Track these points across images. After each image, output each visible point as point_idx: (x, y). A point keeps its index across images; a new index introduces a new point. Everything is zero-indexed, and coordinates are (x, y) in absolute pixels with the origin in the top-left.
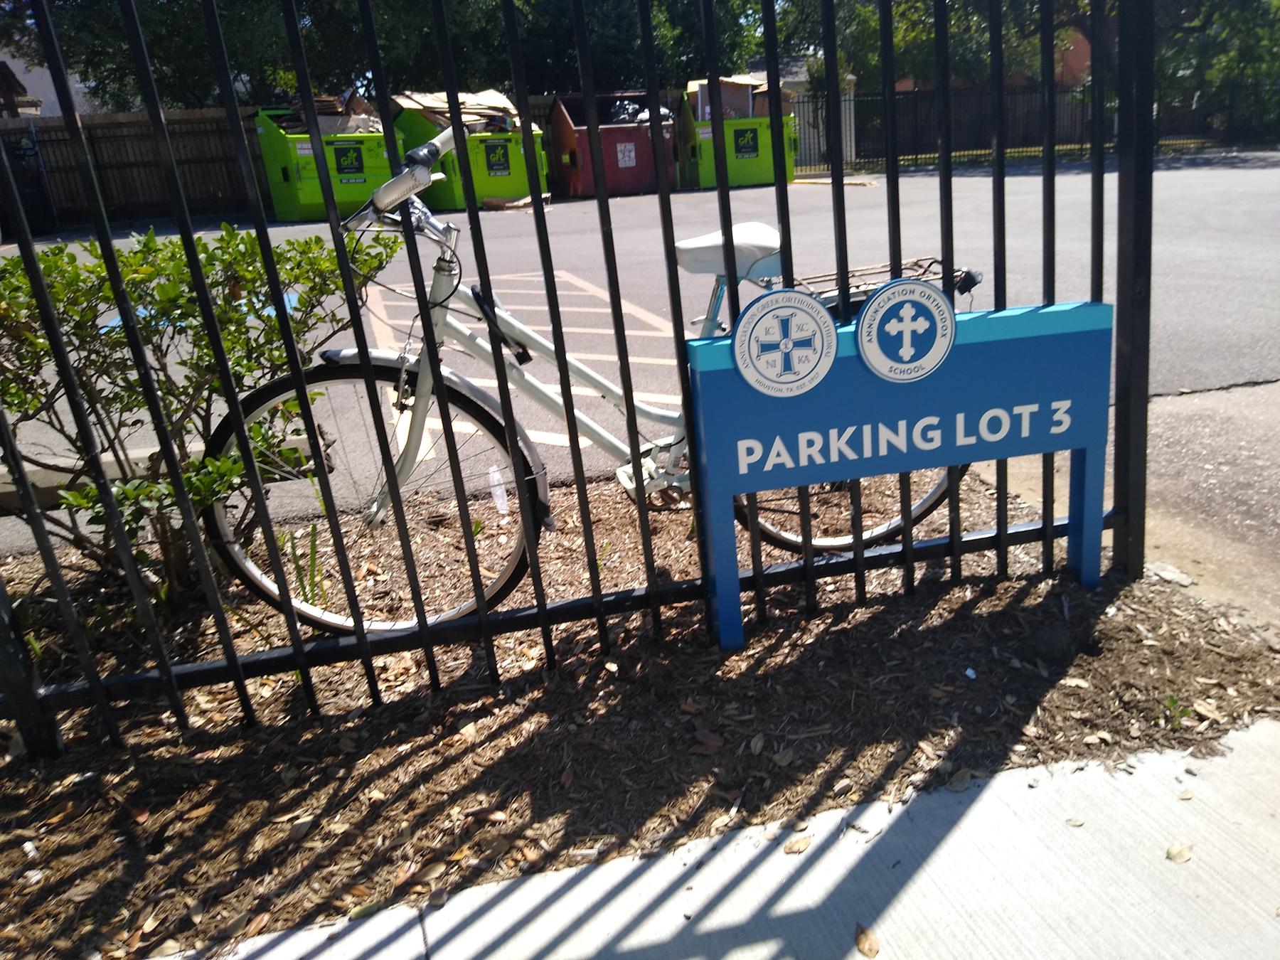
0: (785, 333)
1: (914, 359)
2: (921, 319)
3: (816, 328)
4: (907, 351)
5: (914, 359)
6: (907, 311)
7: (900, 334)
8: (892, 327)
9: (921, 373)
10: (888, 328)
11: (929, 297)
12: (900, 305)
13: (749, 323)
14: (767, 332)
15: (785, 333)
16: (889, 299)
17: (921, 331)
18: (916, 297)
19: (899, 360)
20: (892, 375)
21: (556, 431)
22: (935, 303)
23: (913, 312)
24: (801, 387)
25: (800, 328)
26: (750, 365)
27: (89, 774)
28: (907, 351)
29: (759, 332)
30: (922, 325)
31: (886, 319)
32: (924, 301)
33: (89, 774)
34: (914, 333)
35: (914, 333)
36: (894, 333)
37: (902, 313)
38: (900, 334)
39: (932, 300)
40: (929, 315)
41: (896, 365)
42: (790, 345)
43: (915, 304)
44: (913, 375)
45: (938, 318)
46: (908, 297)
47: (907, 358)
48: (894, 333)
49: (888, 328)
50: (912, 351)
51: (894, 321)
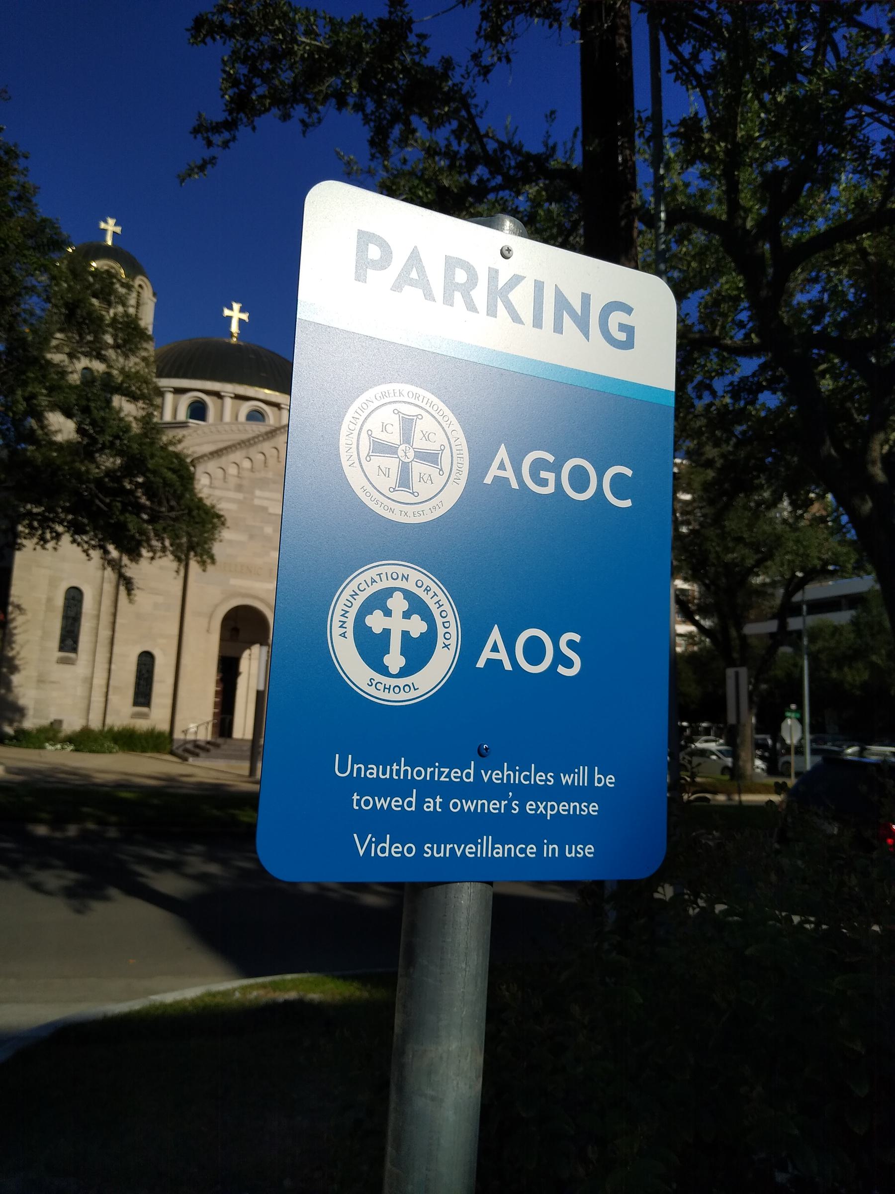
0: (407, 437)
1: (404, 672)
2: (416, 618)
3: (446, 443)
4: (395, 660)
5: (404, 672)
6: (398, 603)
7: (387, 632)
8: (376, 622)
9: (413, 694)
10: (370, 621)
11: (427, 590)
12: (388, 592)
13: (362, 409)
14: (384, 428)
15: (389, 450)
16: (374, 581)
17: (415, 634)
18: (410, 586)
19: (384, 670)
20: (372, 690)
21: (310, 323)
22: (436, 599)
23: (405, 606)
24: (459, 471)
25: (426, 437)
26: (357, 464)
27: (785, 187)
28: (395, 660)
29: (373, 424)
30: (417, 627)
31: (367, 608)
32: (420, 592)
33: (785, 187)
34: (405, 634)
35: (405, 634)
36: (377, 630)
37: (390, 603)
38: (387, 632)
39: (431, 594)
40: (427, 616)
41: (378, 677)
42: (411, 454)
43: (408, 595)
44: (403, 696)
45: (439, 621)
46: (399, 584)
47: (394, 670)
48: (377, 630)
49: (370, 621)
50: (402, 661)
51: (378, 613)
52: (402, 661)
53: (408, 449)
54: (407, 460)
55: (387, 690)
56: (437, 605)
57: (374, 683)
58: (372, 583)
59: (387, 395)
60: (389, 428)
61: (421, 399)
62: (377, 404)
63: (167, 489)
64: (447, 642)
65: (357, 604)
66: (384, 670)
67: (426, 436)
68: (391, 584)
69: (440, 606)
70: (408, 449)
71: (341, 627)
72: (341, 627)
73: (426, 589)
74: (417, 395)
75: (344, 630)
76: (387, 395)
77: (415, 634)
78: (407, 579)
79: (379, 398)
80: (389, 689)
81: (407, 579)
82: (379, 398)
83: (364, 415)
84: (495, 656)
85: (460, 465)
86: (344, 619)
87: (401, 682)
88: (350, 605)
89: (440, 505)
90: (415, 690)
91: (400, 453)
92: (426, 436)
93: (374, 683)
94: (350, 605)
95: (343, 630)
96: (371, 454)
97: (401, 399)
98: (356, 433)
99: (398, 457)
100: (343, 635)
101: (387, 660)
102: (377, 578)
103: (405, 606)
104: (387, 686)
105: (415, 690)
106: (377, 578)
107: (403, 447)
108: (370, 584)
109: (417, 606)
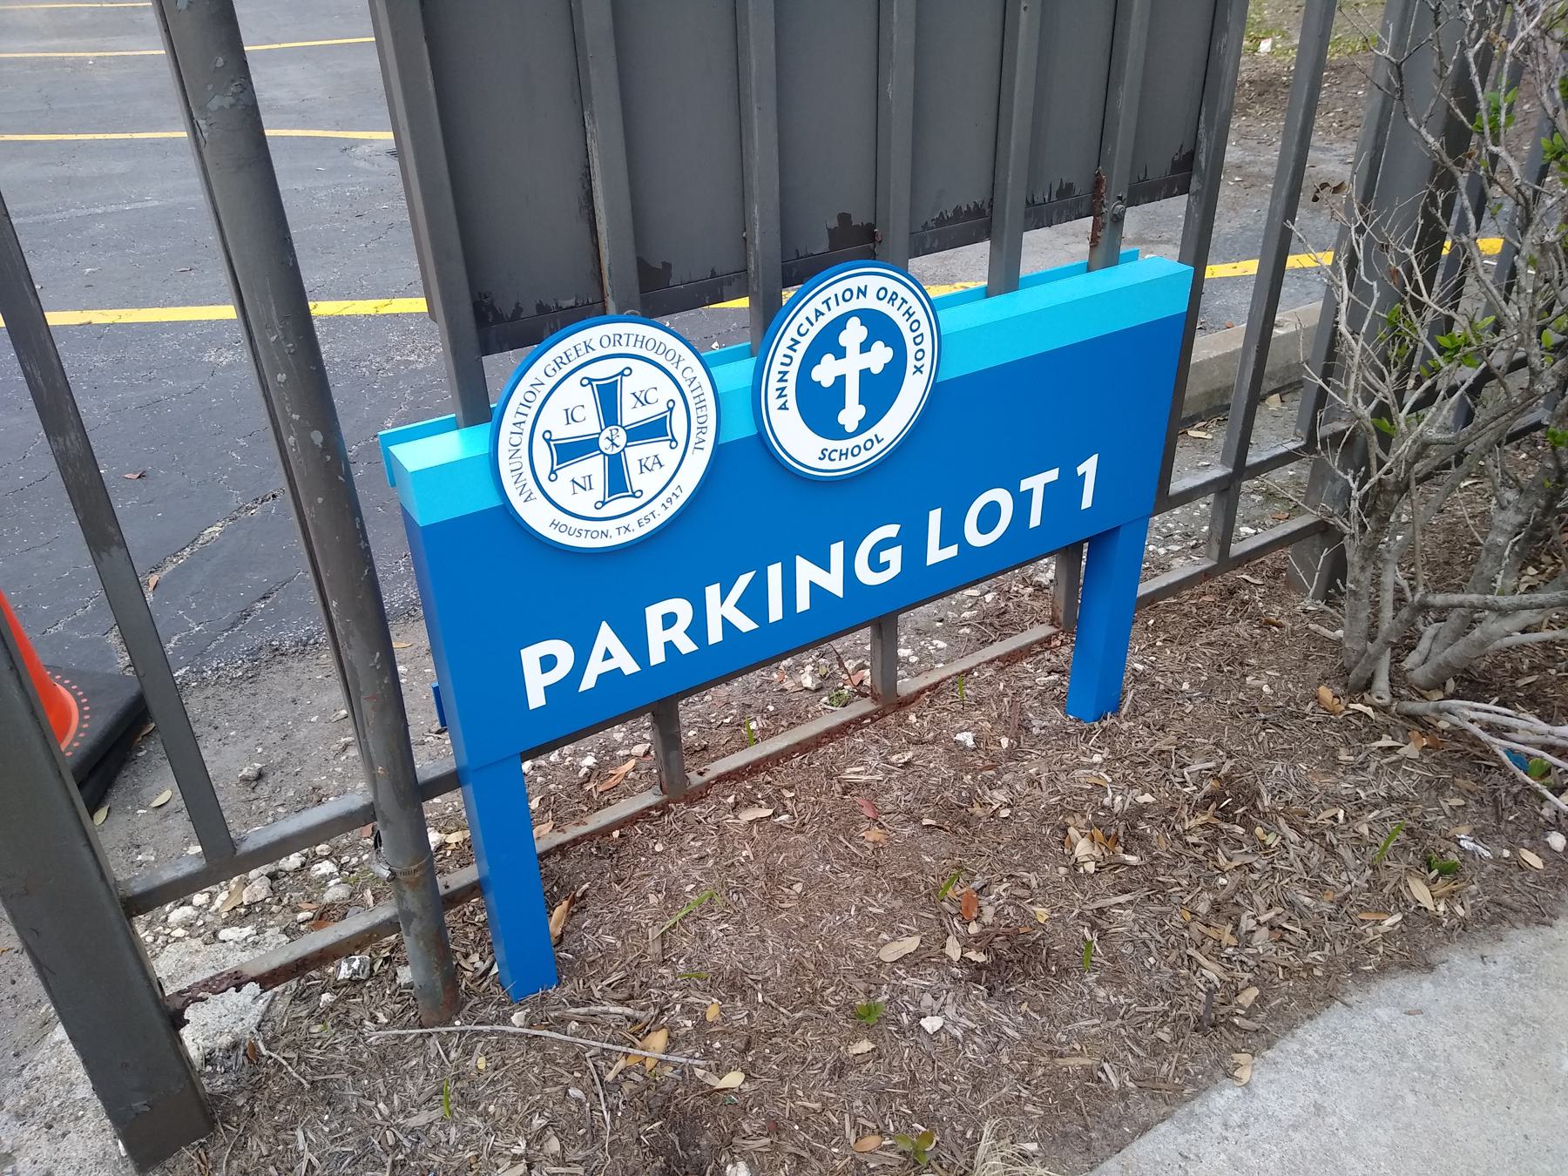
2: (878, 346)
6: (854, 333)
12: (840, 324)
14: (570, 417)
18: (870, 302)
31: (812, 358)
32: (884, 307)
37: (844, 339)
48: (827, 382)
50: (861, 412)
51: (828, 359)
54: (616, 450)
55: (843, 457)
58: (817, 317)
59: (565, 360)
62: (550, 383)
63: (598, 995)
65: (798, 357)
73: (891, 298)
82: (553, 373)
83: (532, 413)
84: (609, 666)
91: (604, 444)
92: (642, 399)
93: (827, 453)
95: (782, 400)
97: (592, 355)
98: (524, 447)
103: (862, 333)
104: (844, 452)
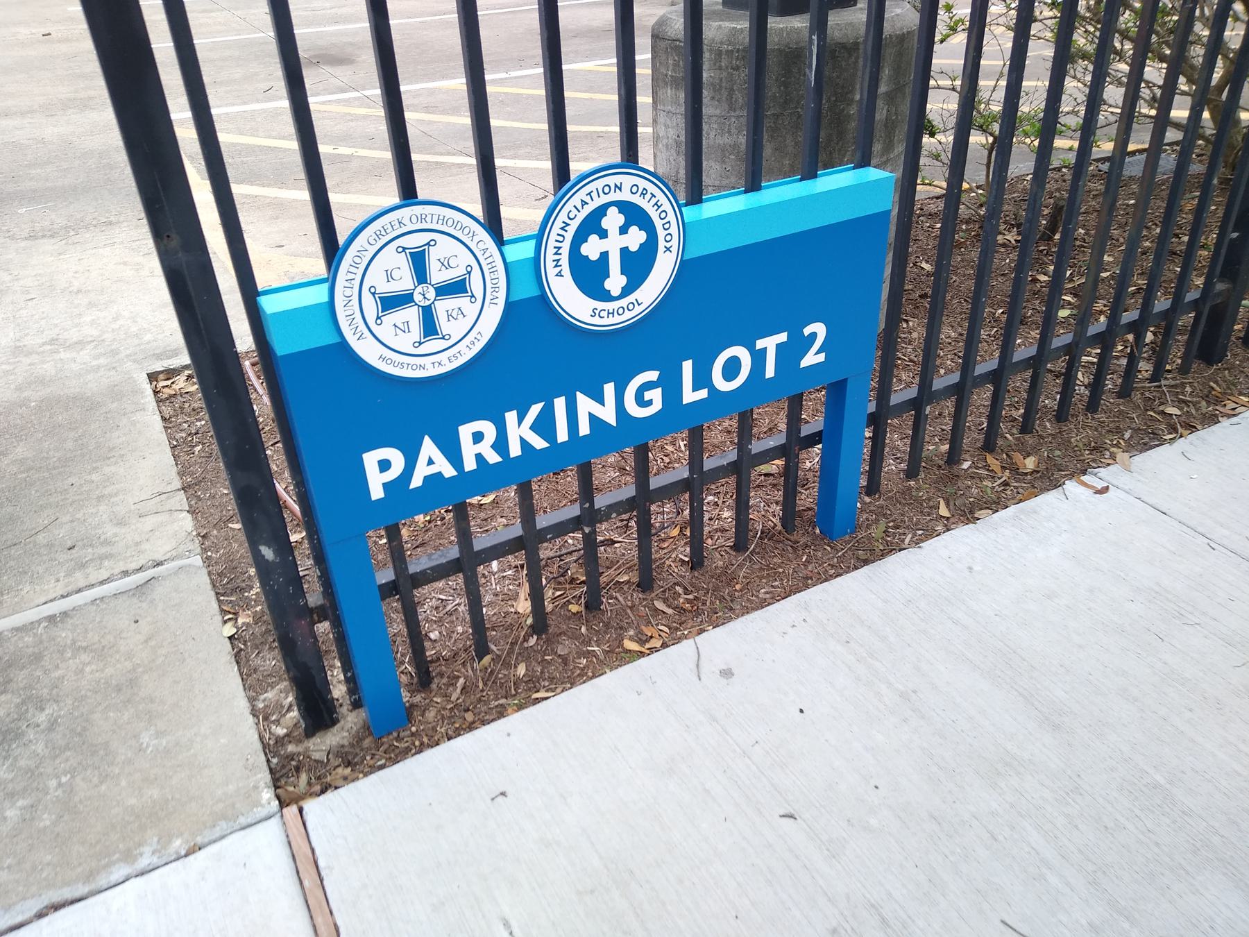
1: (626, 291)
2: (634, 230)
4: (616, 282)
5: (626, 291)
6: (613, 220)
7: (605, 256)
8: (592, 248)
9: (638, 309)
12: (601, 211)
14: (389, 276)
17: (634, 248)
18: (625, 196)
20: (596, 321)
22: (654, 200)
25: (446, 265)
28: (616, 282)
31: (580, 237)
34: (624, 251)
35: (624, 251)
36: (594, 257)
37: (605, 223)
38: (605, 256)
39: (648, 196)
42: (431, 294)
43: (623, 206)
48: (594, 257)
50: (623, 280)
51: (593, 238)
52: (623, 280)
53: (425, 289)
54: (427, 303)
55: (611, 315)
56: (656, 207)
57: (597, 312)
59: (383, 233)
60: (396, 274)
61: (428, 219)
62: (373, 250)
64: (668, 245)
65: (569, 236)
66: (606, 296)
67: (446, 263)
68: (605, 199)
69: (659, 207)
70: (425, 289)
71: (556, 266)
72: (556, 266)
73: (642, 193)
74: (424, 216)
75: (558, 269)
76: (383, 233)
77: (634, 248)
78: (620, 189)
79: (374, 242)
80: (613, 313)
81: (620, 189)
82: (374, 242)
85: (494, 282)
86: (557, 257)
87: (624, 302)
88: (561, 239)
89: (479, 337)
90: (639, 305)
92: (446, 263)
93: (597, 312)
94: (561, 239)
96: (380, 314)
97: (404, 230)
99: (416, 304)
100: (559, 275)
101: (608, 284)
102: (587, 199)
103: (621, 219)
105: (639, 305)
106: (587, 199)
107: (419, 289)
108: (580, 208)
109: (634, 216)
